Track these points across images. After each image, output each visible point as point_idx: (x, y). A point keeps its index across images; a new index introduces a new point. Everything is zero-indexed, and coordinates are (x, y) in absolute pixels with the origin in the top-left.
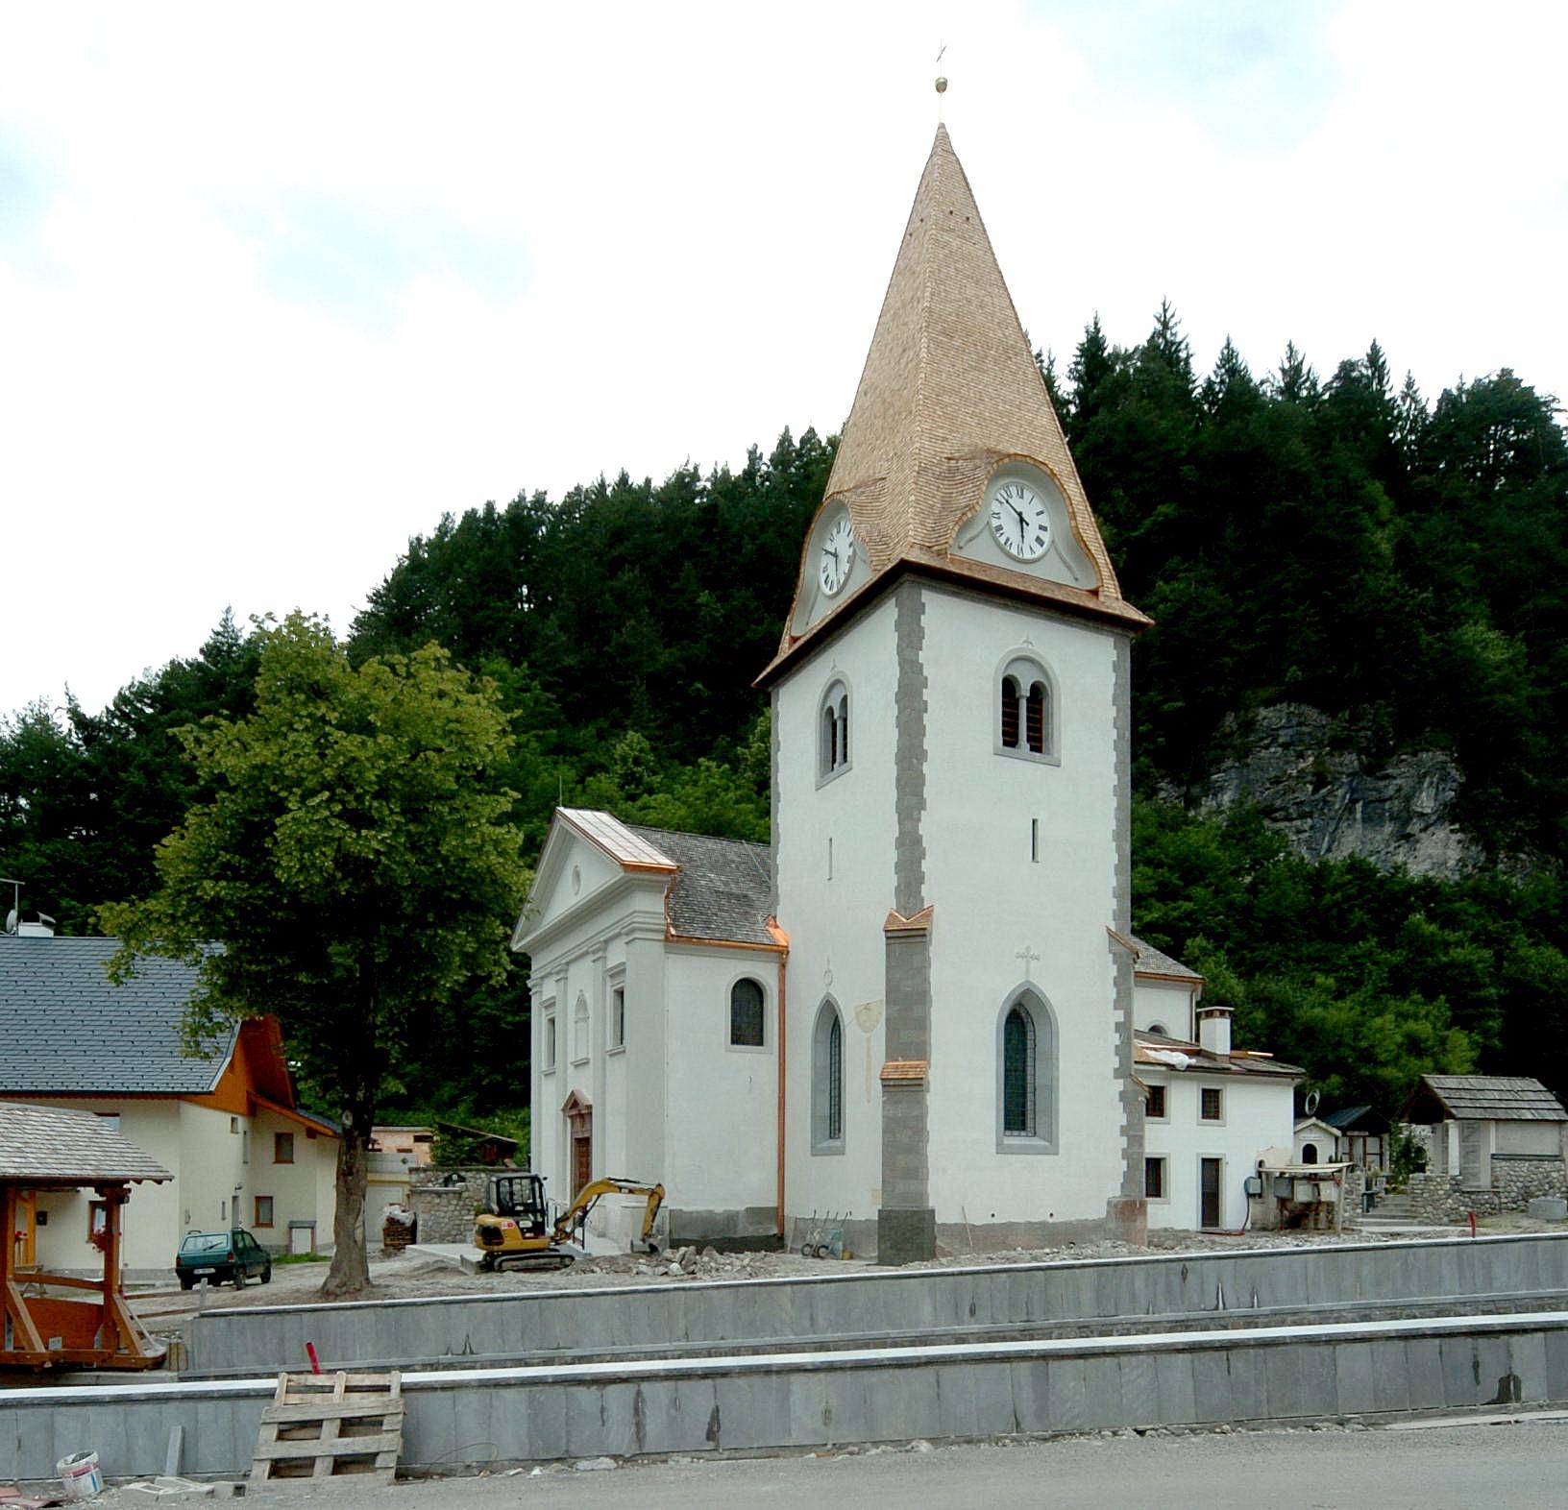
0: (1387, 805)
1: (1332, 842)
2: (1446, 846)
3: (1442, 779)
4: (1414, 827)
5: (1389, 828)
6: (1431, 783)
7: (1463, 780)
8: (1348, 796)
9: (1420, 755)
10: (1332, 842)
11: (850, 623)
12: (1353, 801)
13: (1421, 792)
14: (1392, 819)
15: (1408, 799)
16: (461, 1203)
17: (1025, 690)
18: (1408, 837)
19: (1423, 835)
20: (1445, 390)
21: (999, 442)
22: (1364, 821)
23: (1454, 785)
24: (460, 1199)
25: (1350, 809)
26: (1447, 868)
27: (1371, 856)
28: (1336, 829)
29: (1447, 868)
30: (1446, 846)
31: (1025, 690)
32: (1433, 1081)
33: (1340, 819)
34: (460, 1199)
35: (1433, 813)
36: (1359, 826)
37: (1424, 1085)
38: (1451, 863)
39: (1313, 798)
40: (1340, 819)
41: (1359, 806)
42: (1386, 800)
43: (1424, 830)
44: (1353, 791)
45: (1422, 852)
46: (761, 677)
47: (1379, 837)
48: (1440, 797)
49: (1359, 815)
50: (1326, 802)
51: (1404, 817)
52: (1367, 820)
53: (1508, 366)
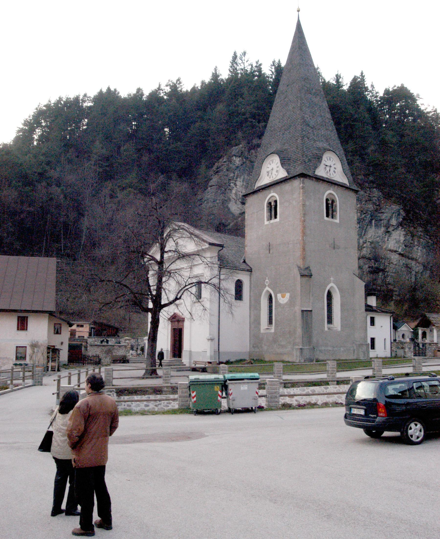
0: (382, 222)
1: (365, 232)
2: (400, 236)
3: (399, 215)
4: (390, 229)
5: (383, 229)
6: (395, 215)
7: (404, 215)
8: (370, 218)
9: (392, 206)
10: (365, 232)
11: (431, 440)
12: (372, 220)
13: (392, 218)
14: (384, 226)
15: (389, 221)
16: (126, 349)
17: (330, 216)
18: (388, 232)
19: (393, 232)
20: (202, 81)
21: (29, 258)
22: (375, 226)
23: (402, 217)
24: (126, 348)
25: (370, 222)
26: (400, 243)
27: (378, 238)
28: (366, 228)
29: (400, 243)
30: (400, 236)
31: (330, 216)
32: (428, 315)
33: (368, 225)
34: (126, 348)
35: (396, 225)
36: (373, 227)
37: (425, 316)
38: (402, 241)
39: (361, 217)
40: (368, 225)
41: (373, 221)
42: (381, 220)
43: (393, 230)
44: (371, 216)
45: (393, 237)
46: (68, 485)
47: (380, 232)
48: (398, 220)
49: (373, 224)
50: (364, 220)
51: (387, 226)
52: (376, 226)
53: (203, 79)
